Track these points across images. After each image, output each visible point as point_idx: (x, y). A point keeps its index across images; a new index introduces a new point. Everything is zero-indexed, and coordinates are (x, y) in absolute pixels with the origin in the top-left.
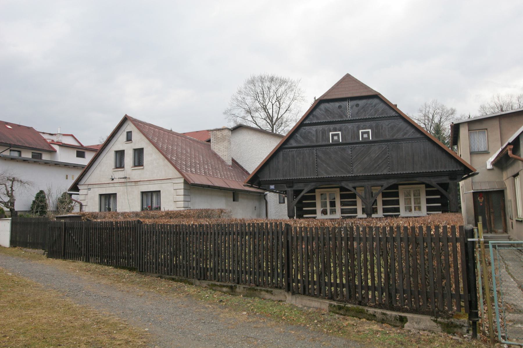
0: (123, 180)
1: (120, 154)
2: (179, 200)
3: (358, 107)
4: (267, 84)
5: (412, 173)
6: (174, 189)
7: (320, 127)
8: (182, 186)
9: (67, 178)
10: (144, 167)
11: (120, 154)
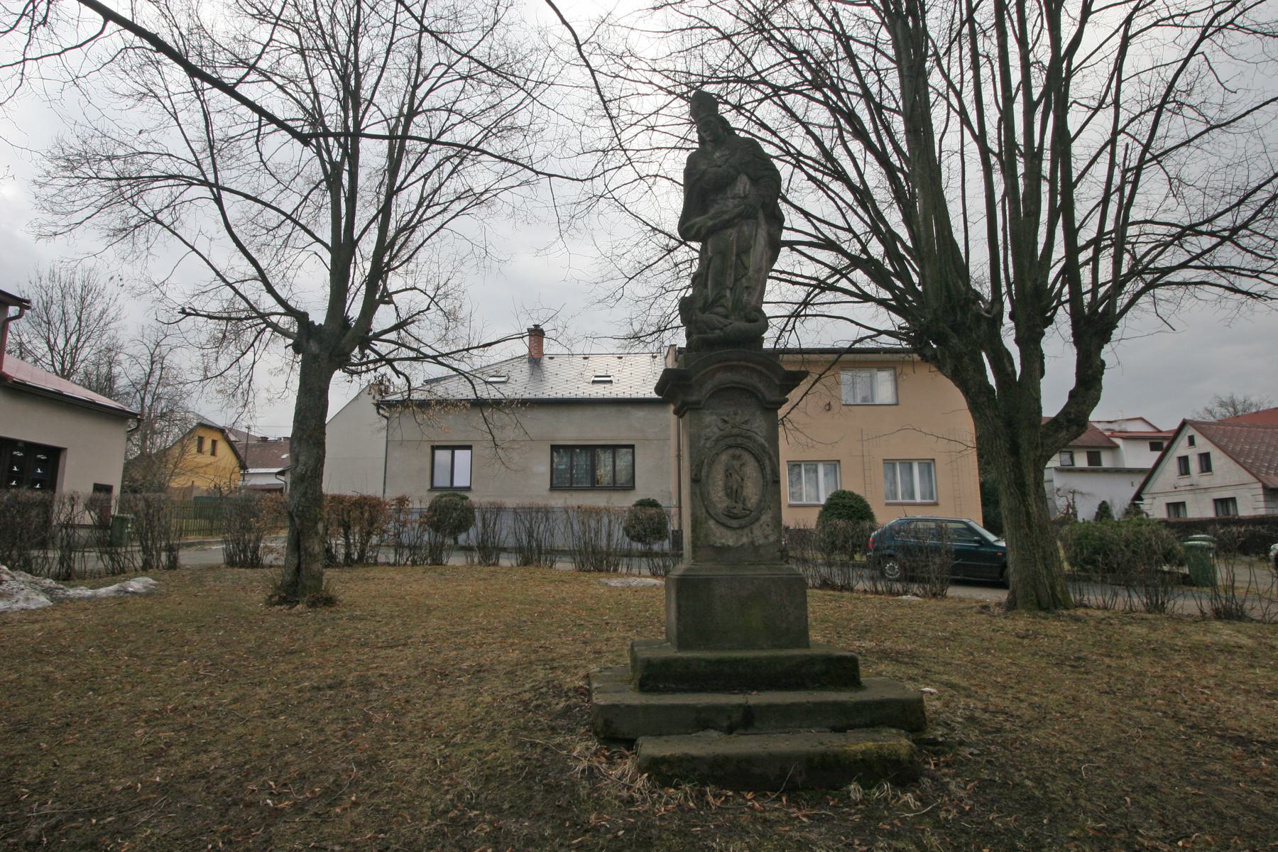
1: (1184, 461)
8: (1261, 491)
11: (1184, 461)
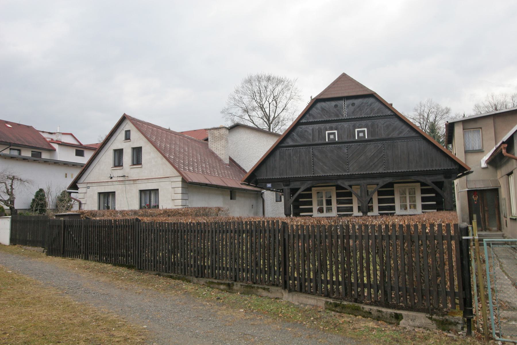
0: (122, 179)
1: (119, 153)
2: (177, 199)
3: (354, 106)
4: (264, 83)
5: (407, 172)
6: (172, 188)
7: (316, 126)
8: (180, 184)
9: (66, 177)
10: (142, 166)
11: (119, 153)
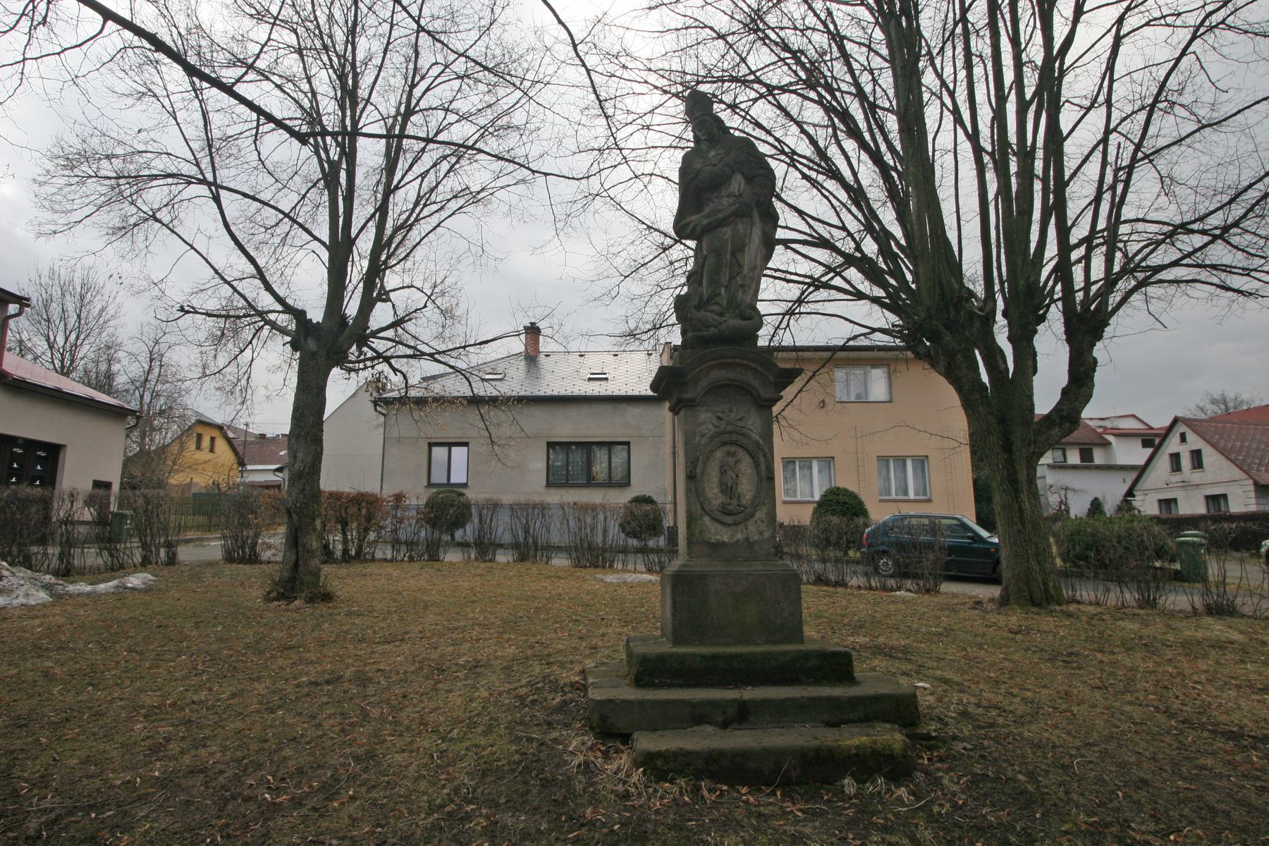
1: (1175, 458)
8: (1252, 488)
11: (1175, 458)
